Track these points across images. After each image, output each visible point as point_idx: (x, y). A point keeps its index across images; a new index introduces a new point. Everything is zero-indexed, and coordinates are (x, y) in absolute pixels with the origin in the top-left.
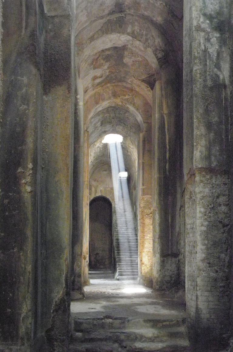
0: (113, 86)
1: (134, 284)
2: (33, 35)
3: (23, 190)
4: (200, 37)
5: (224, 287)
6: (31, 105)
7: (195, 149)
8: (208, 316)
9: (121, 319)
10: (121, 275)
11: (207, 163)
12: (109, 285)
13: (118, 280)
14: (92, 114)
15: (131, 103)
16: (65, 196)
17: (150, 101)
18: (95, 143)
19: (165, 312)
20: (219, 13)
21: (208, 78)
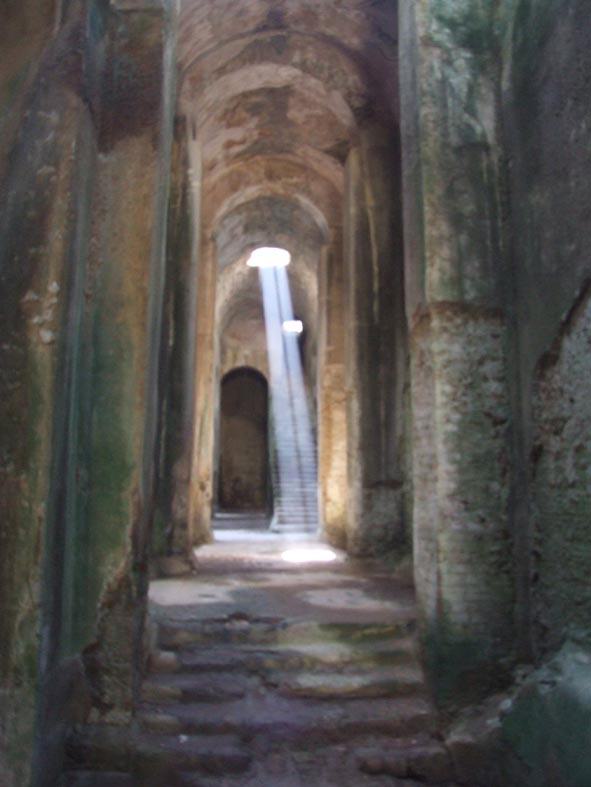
0: (268, 160)
1: (310, 541)
2: (76, 36)
3: (34, 339)
4: (434, 58)
5: (499, 553)
6: (63, 166)
7: (428, 263)
8: (464, 617)
9: (267, 621)
10: (282, 522)
11: (455, 293)
12: (254, 543)
13: (277, 532)
14: (223, 210)
15: (304, 190)
16: (136, 355)
17: (341, 190)
18: (234, 266)
19: (368, 605)
20: (469, 17)
21: (451, 130)
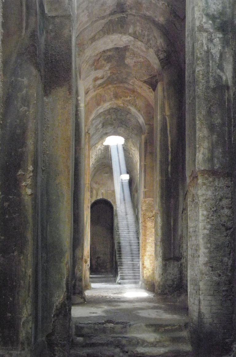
0: (115, 87)
1: (136, 288)
2: (33, 36)
3: (23, 193)
4: (203, 38)
5: (227, 291)
6: (31, 106)
7: (197, 151)
8: (211, 320)
9: (122, 323)
10: (122, 279)
11: (210, 166)
12: (110, 289)
13: (120, 284)
14: (93, 116)
15: (133, 104)
16: (66, 199)
17: (152, 103)
18: (97, 145)
19: (167, 317)
20: (222, 14)
21: (211, 79)
